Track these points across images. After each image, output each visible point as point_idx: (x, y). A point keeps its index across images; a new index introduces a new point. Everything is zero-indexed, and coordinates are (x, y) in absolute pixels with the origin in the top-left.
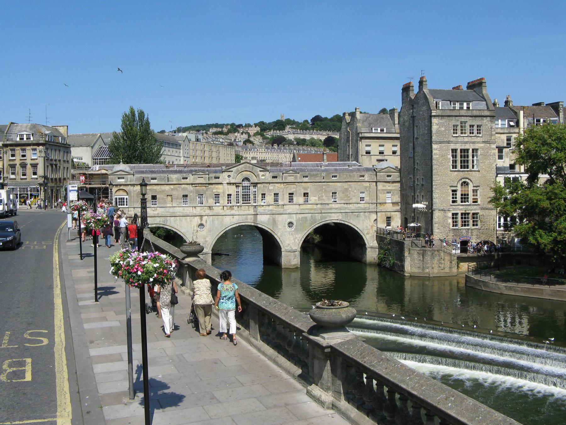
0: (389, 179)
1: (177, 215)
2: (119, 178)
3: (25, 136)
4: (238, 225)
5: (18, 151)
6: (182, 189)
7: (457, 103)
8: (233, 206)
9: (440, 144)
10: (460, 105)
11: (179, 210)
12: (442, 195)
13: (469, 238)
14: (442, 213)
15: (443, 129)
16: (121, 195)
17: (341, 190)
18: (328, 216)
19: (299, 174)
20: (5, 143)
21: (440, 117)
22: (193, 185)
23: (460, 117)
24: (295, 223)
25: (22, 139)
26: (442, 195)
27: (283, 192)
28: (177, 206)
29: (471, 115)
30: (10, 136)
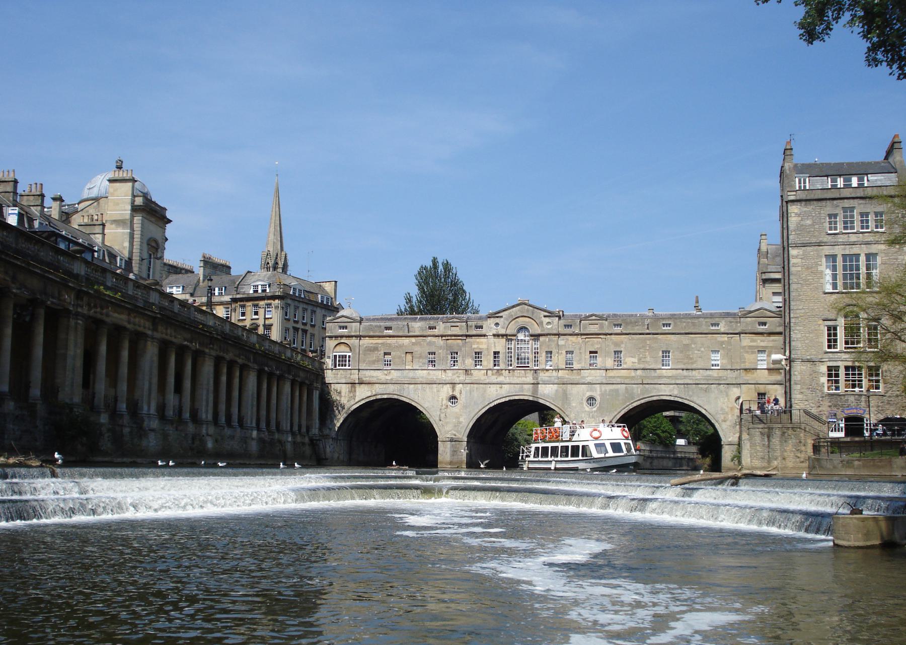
0: (762, 328)
1: (419, 382)
2: (341, 327)
3: (260, 287)
4: (507, 399)
5: (249, 308)
6: (427, 344)
7: (839, 179)
8: (502, 370)
9: (803, 248)
10: (844, 182)
11: (422, 375)
12: (807, 335)
13: (861, 412)
14: (809, 366)
15: (809, 222)
16: (342, 351)
17: (678, 348)
18: (655, 389)
19: (606, 320)
20: (235, 297)
21: (803, 203)
22: (444, 338)
23: (841, 201)
24: (598, 398)
25: (256, 291)
26: (807, 335)
27: (580, 349)
28: (420, 368)
29: (862, 195)
30: (242, 288)
